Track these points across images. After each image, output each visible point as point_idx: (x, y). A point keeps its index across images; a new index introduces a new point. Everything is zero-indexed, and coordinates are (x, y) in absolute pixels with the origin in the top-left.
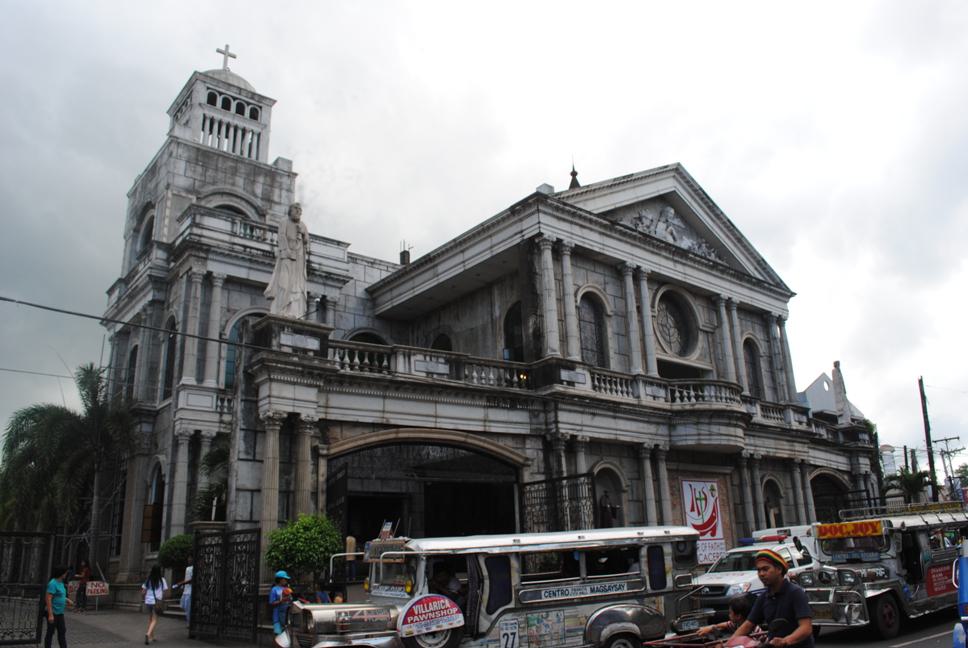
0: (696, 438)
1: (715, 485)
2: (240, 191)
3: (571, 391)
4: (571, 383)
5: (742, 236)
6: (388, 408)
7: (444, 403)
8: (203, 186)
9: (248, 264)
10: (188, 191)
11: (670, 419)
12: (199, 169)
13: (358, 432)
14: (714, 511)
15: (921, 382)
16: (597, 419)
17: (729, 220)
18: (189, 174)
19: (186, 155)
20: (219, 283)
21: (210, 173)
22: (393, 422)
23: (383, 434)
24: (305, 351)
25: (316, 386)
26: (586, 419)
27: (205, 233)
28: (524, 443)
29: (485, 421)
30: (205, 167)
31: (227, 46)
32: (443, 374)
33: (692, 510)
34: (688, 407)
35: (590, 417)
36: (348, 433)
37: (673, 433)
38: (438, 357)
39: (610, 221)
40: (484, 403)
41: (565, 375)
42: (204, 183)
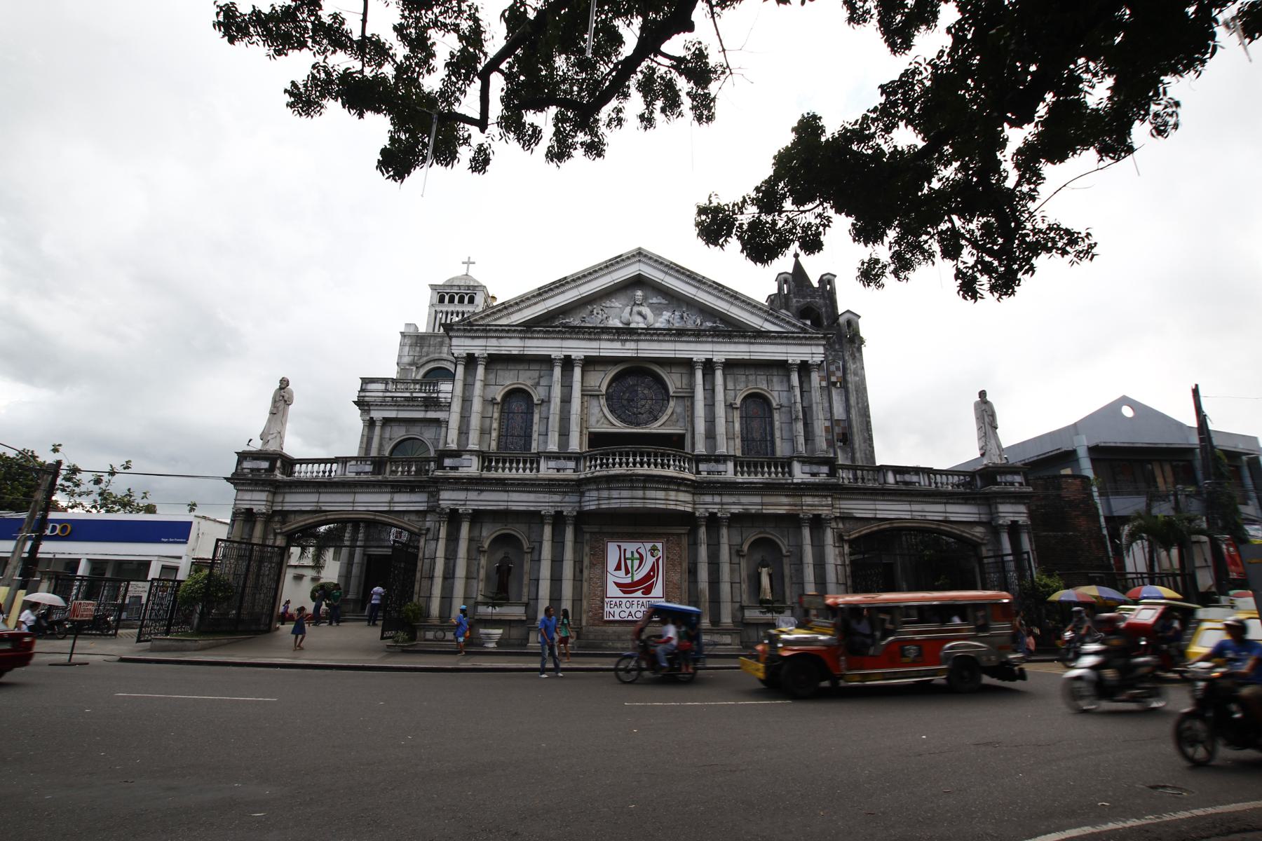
0: (596, 502)
1: (659, 546)
2: (444, 356)
3: (452, 474)
4: (455, 468)
5: (737, 292)
6: (321, 500)
7: (360, 493)
8: (419, 359)
9: (396, 408)
10: (410, 364)
11: (578, 486)
12: (418, 349)
13: (306, 517)
14: (652, 569)
15: (1196, 392)
16: (485, 493)
17: (714, 282)
18: (411, 353)
19: (409, 342)
20: (378, 424)
21: (425, 349)
22: (324, 508)
23: (317, 517)
24: (259, 470)
25: (267, 491)
26: (473, 495)
27: (367, 394)
28: (425, 517)
29: (390, 503)
30: (422, 347)
31: (469, 258)
32: (368, 472)
33: (618, 568)
34: (589, 475)
35: (476, 493)
36: (300, 518)
37: (584, 499)
38: (366, 461)
39: (529, 328)
40: (389, 489)
41: (448, 462)
42: (420, 357)
